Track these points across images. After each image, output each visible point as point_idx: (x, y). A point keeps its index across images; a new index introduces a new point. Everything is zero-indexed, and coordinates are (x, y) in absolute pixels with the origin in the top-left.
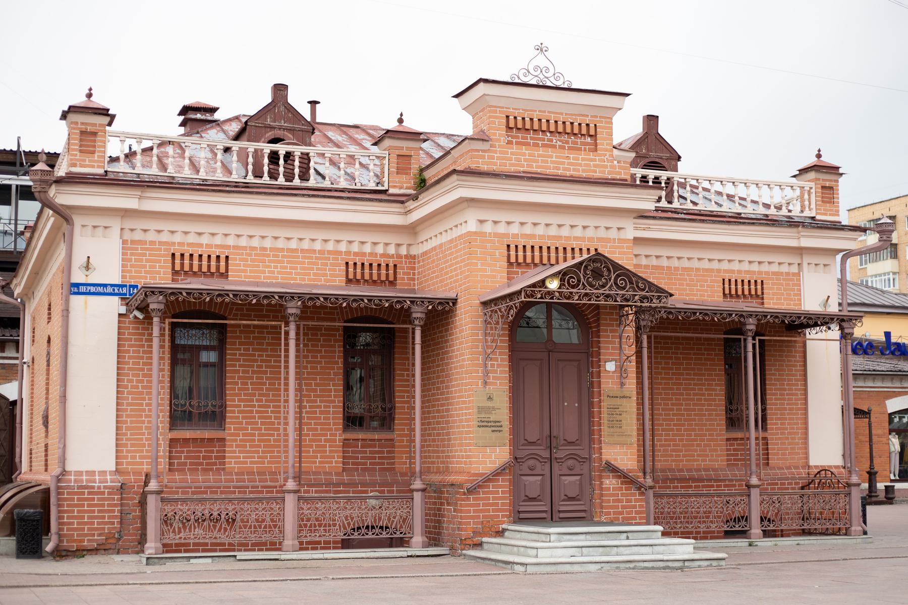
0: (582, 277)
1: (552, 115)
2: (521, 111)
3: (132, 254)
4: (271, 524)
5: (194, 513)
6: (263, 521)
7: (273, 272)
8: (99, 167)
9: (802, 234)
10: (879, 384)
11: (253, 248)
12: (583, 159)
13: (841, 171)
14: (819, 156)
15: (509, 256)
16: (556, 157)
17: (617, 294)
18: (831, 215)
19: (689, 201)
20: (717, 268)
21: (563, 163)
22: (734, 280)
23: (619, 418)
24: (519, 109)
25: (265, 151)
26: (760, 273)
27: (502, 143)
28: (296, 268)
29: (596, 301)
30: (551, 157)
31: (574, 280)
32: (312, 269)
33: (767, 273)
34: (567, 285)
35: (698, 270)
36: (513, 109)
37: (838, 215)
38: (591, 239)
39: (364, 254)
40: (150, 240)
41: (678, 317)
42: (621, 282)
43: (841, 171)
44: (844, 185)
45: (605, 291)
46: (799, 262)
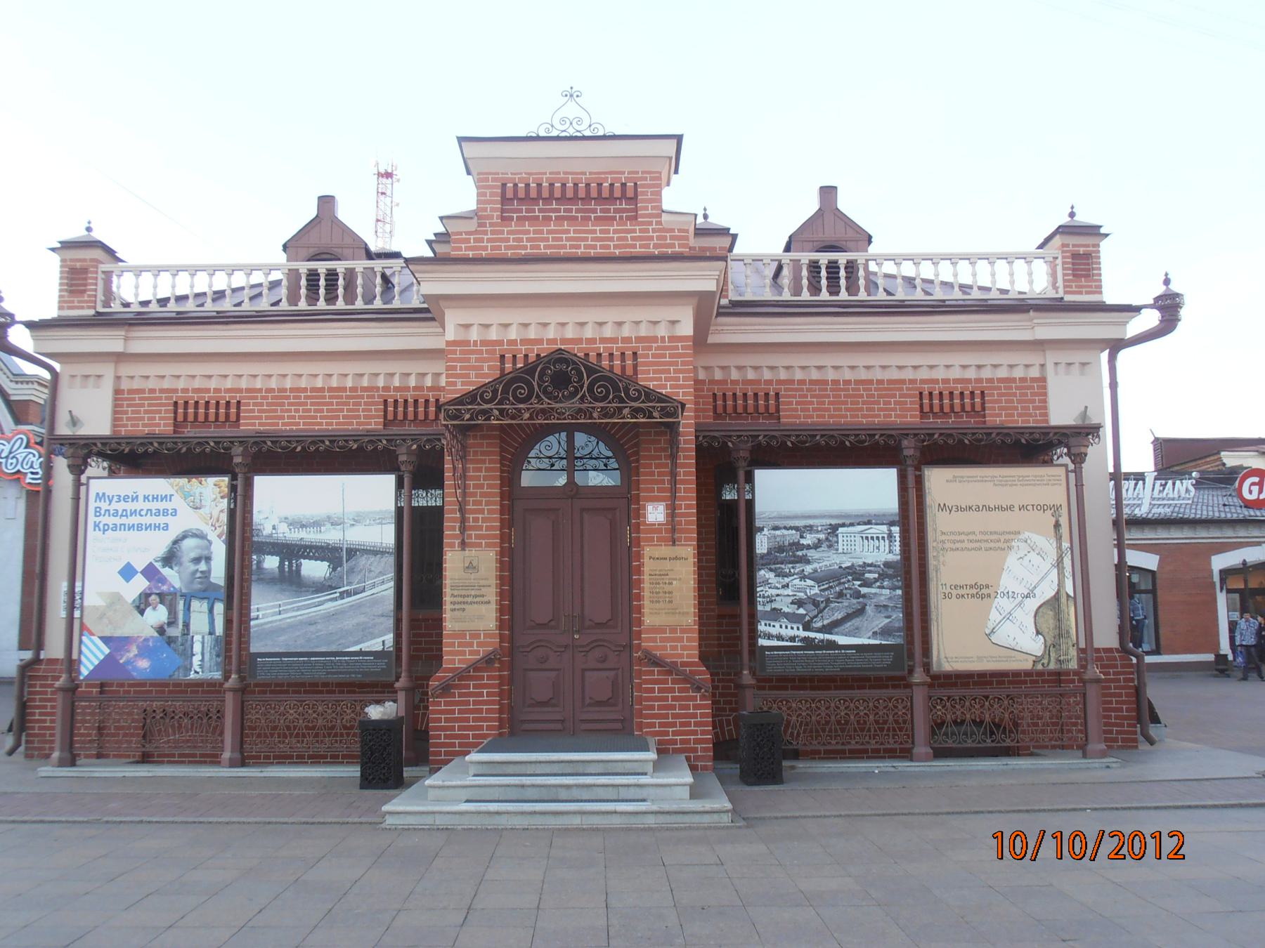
0: (536, 387)
1: (570, 176)
2: (524, 175)
3: (128, 406)
4: (838, 727)
5: (207, 715)
6: (885, 722)
7: (294, 417)
8: (89, 307)
9: (1035, 321)
10: (1204, 534)
11: (269, 390)
12: (615, 232)
13: (1102, 231)
14: (1072, 215)
15: (921, 406)
16: (575, 232)
17: (593, 408)
18: (1087, 293)
19: (881, 290)
20: (911, 377)
21: (586, 239)
22: (927, 392)
23: (667, 588)
24: (521, 174)
25: (802, 262)
26: (979, 380)
27: (495, 220)
28: (322, 411)
29: (558, 419)
30: (568, 232)
31: (523, 391)
32: (342, 410)
33: (990, 380)
34: (511, 398)
35: (880, 382)
36: (512, 174)
37: (1101, 293)
38: (627, 340)
39: (408, 389)
40: (150, 387)
41: (786, 442)
42: (599, 390)
43: (1102, 231)
44: (1108, 253)
45: (573, 403)
46: (1042, 363)
